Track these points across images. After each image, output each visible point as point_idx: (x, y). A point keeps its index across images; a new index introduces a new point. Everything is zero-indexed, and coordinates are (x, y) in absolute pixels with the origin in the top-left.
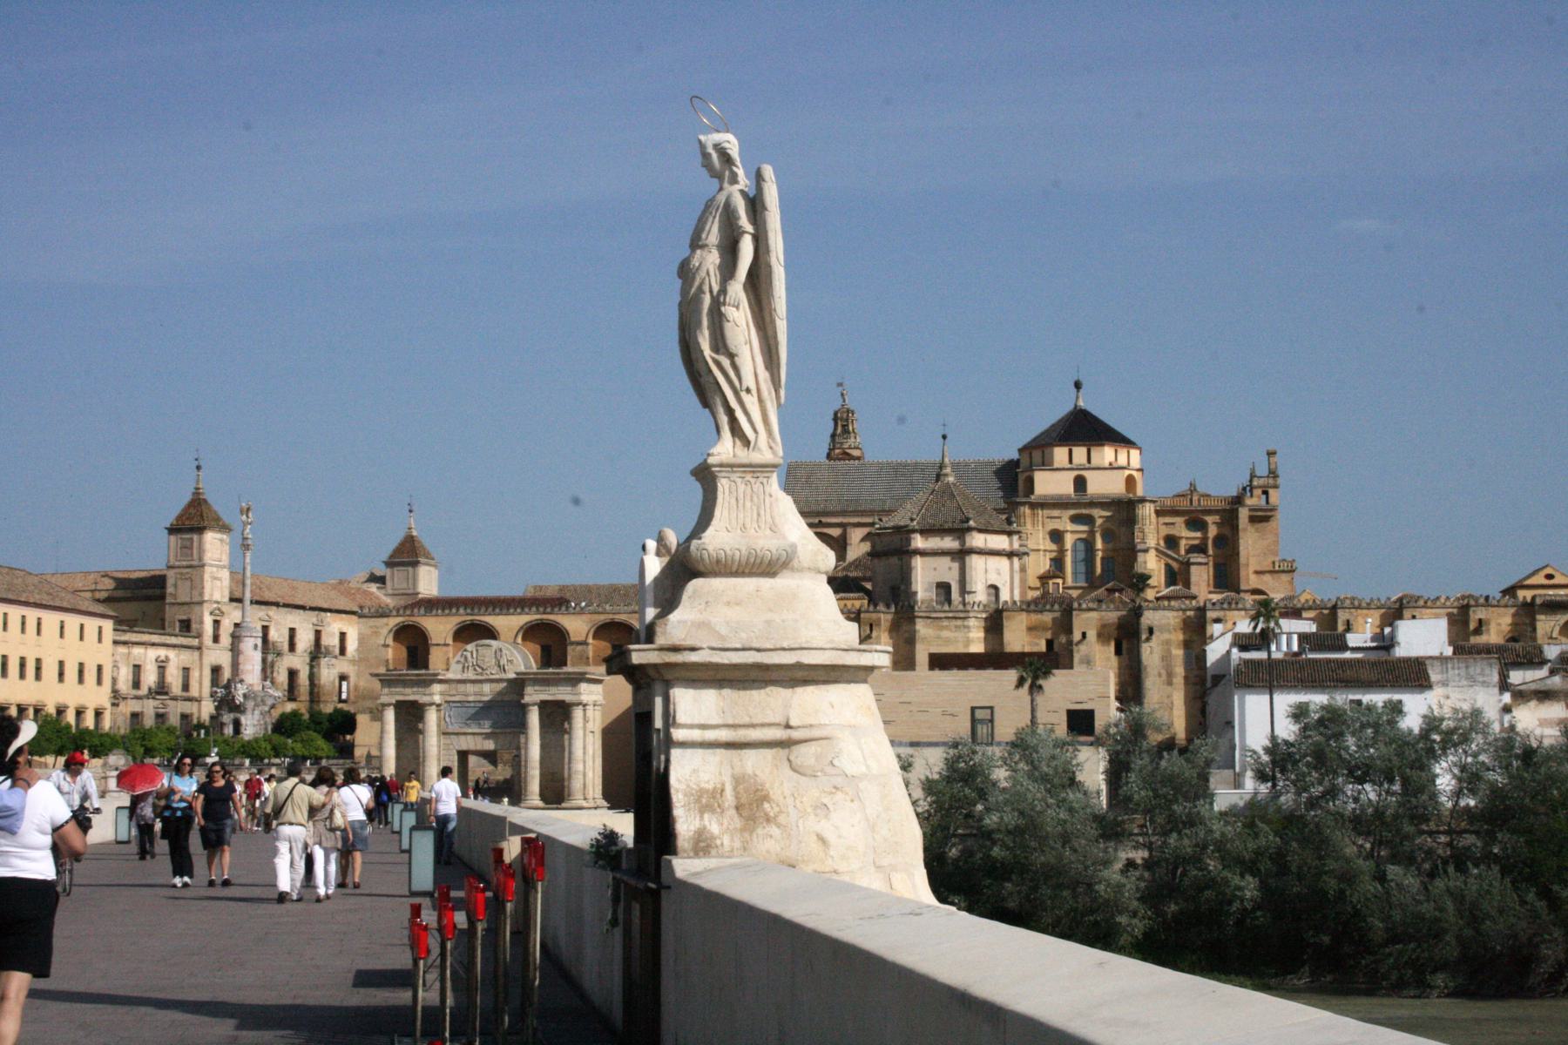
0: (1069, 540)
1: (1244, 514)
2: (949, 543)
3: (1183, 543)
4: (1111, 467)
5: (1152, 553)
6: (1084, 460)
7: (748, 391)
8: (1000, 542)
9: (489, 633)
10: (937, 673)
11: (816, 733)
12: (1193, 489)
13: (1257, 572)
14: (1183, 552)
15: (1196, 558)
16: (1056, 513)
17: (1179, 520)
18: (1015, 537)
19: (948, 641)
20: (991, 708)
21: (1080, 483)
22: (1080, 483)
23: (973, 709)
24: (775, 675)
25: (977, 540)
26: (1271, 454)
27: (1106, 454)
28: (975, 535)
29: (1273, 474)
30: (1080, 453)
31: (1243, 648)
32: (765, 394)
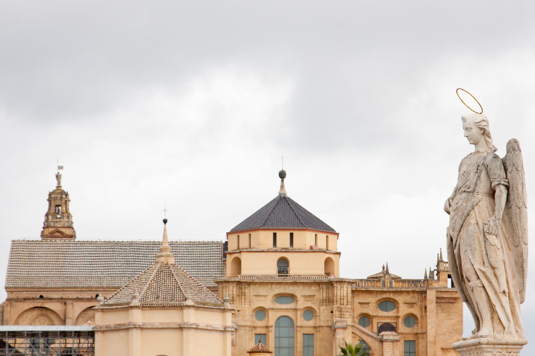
0: (273, 317)
1: (431, 295)
2: (170, 317)
3: (375, 321)
4: (312, 250)
5: (350, 330)
6: (287, 245)
7: (504, 292)
8: (214, 319)
12: (386, 271)
13: (442, 349)
14: (375, 330)
15: (387, 335)
16: (262, 290)
17: (373, 300)
18: (229, 315)
21: (283, 265)
22: (283, 265)
25: (191, 317)
27: (305, 239)
28: (192, 311)
30: (283, 238)
32: (513, 295)
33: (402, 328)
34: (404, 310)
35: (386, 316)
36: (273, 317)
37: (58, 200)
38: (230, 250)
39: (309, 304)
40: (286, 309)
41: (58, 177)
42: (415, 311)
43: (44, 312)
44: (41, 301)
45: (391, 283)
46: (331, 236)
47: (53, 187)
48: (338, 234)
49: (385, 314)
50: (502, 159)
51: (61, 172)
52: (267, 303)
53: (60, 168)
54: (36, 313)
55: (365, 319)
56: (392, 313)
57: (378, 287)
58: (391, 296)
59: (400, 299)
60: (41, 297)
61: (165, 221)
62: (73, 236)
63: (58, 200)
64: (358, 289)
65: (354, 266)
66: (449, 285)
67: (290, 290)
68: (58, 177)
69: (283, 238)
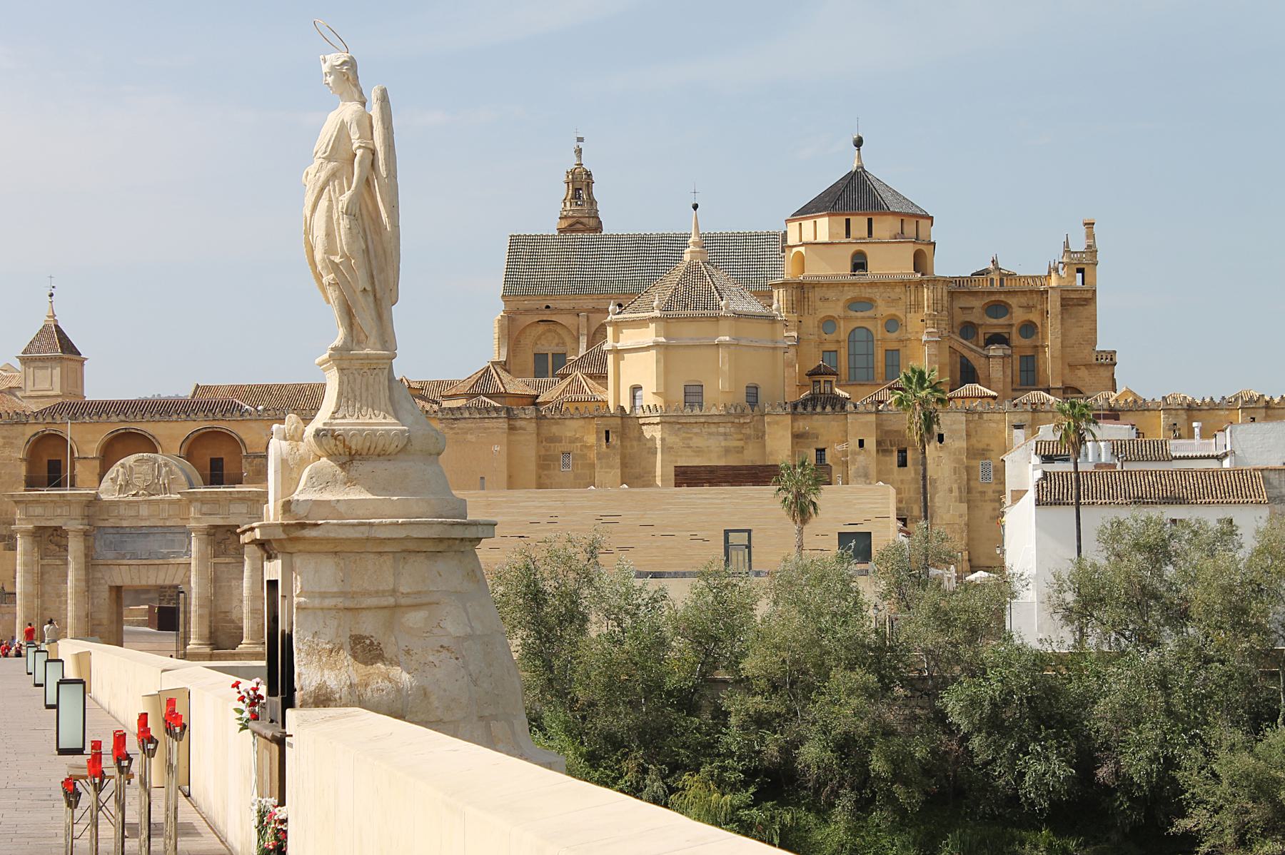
3: (981, 332)
9: (146, 443)
10: (684, 489)
11: (425, 600)
14: (982, 343)
15: (995, 350)
16: (831, 294)
17: (978, 303)
19: (699, 451)
20: (749, 531)
21: (859, 264)
22: (859, 264)
23: (727, 532)
24: (330, 547)
26: (1089, 225)
29: (1092, 250)
31: (1048, 459)
33: (1016, 339)
34: (1019, 316)
35: (996, 324)
36: (843, 331)
37: (580, 185)
38: (790, 242)
39: (893, 311)
40: (863, 318)
41: (579, 152)
42: (1035, 317)
43: (552, 327)
44: (548, 311)
45: (1001, 280)
46: (921, 222)
47: (571, 163)
48: (934, 244)
49: (994, 321)
50: (97, 497)
51: (581, 145)
52: (836, 310)
53: (580, 140)
54: (542, 327)
55: (968, 330)
56: (1002, 321)
57: (984, 286)
58: (1002, 298)
59: (1013, 301)
60: (548, 307)
61: (695, 207)
62: (598, 228)
63: (580, 185)
64: (957, 289)
65: (951, 262)
66: (1079, 282)
67: (867, 293)
68: (579, 152)
69: (859, 224)
